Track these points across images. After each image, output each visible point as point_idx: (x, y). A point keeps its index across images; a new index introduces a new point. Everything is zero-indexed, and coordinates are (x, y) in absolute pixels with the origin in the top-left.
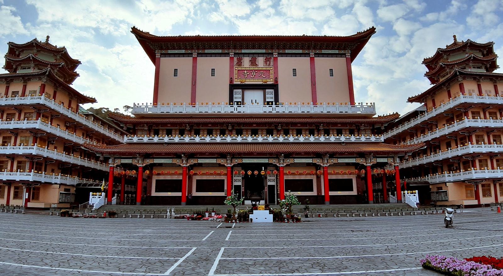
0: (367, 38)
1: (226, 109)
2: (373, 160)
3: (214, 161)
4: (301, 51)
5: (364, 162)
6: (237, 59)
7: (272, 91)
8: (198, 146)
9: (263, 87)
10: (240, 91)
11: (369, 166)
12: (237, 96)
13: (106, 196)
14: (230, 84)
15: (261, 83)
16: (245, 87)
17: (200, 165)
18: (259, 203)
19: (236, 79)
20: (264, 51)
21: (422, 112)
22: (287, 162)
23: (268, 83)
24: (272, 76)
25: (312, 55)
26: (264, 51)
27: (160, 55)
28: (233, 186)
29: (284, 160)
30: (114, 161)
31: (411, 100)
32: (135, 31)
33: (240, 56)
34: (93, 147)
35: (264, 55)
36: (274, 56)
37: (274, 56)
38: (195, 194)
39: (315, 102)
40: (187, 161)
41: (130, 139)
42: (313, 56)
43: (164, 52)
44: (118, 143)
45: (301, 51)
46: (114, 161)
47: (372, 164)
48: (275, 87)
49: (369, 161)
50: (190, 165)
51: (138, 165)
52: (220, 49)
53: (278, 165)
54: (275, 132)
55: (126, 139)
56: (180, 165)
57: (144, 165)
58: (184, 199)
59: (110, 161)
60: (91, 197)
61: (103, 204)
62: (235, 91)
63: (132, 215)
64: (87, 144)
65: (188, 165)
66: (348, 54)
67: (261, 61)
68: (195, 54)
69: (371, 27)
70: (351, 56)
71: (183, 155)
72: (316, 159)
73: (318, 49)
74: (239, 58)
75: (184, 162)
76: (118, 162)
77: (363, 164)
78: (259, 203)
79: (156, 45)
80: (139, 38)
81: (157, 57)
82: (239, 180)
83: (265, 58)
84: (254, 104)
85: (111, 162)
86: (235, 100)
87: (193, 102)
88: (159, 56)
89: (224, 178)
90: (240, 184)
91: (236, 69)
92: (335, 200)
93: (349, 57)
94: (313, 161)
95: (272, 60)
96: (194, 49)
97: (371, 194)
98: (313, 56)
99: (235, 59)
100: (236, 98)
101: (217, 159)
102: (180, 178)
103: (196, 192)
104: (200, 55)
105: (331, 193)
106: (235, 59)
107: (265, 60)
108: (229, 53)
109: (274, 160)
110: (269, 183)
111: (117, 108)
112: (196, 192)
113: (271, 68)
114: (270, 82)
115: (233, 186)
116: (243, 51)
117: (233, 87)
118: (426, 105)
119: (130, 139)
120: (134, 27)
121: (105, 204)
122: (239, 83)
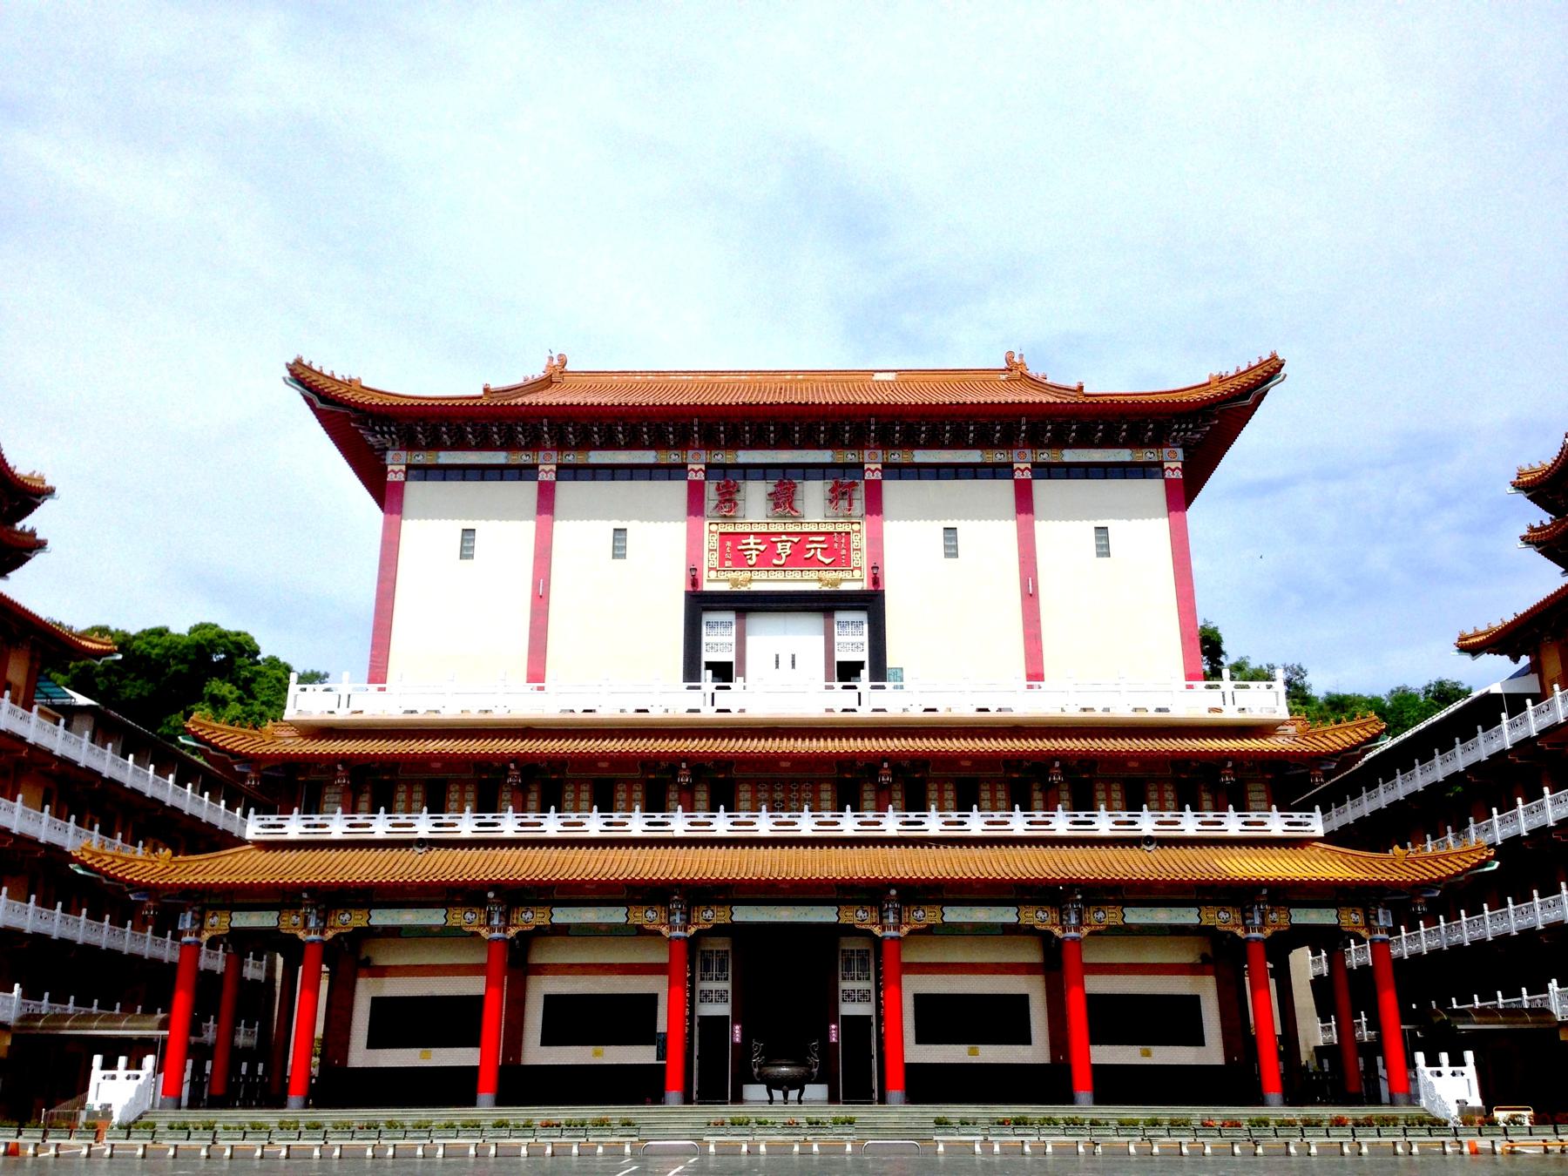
0: (1249, 401)
1: (672, 698)
2: (1274, 916)
3: (616, 916)
4: (499, 458)
5: (1236, 925)
6: (718, 489)
7: (862, 616)
8: (555, 853)
9: (825, 604)
10: (730, 617)
11: (1257, 939)
12: (718, 642)
13: (159, 1068)
14: (687, 593)
15: (815, 587)
16: (745, 605)
17: (563, 930)
18: (800, 1095)
19: (713, 574)
20: (824, 456)
21: (1515, 704)
22: (912, 920)
23: (844, 587)
24: (860, 559)
25: (547, 472)
26: (824, 456)
27: (406, 473)
28: (696, 1021)
29: (899, 913)
30: (200, 921)
31: (1471, 648)
32: (303, 377)
33: (730, 479)
34: (119, 862)
35: (828, 471)
36: (868, 476)
37: (868, 476)
38: (536, 1053)
39: (536, 675)
40: (506, 917)
41: (316, 826)
42: (878, 476)
43: (571, 458)
44: (228, 840)
45: (974, 456)
46: (202, 922)
47: (1269, 932)
48: (871, 603)
49: (1257, 921)
50: (519, 934)
51: (301, 935)
52: (649, 448)
53: (877, 930)
54: (868, 796)
55: (253, 828)
56: (476, 934)
57: (330, 934)
58: (488, 1078)
59: (186, 922)
60: (97, 1073)
61: (147, 1107)
62: (708, 617)
63: (288, 1147)
64: (94, 854)
65: (512, 932)
66: (1173, 465)
67: (813, 494)
68: (547, 468)
69: (1266, 357)
70: (1183, 471)
71: (491, 895)
72: (1033, 909)
73: (894, 447)
74: (727, 486)
75: (496, 922)
76: (218, 923)
77: (1233, 934)
78: (800, 1095)
79: (390, 433)
80: (319, 405)
81: (391, 477)
82: (721, 996)
83: (829, 484)
84: (785, 678)
85: (188, 926)
86: (707, 656)
87: (378, 674)
88: (401, 477)
89: (657, 985)
90: (723, 1009)
91: (714, 528)
92: (1117, 1087)
93: (1178, 475)
94: (1022, 915)
95: (860, 494)
96: (545, 449)
97: (1081, 1077)
98: (878, 476)
99: (711, 490)
100: (712, 647)
101: (632, 908)
102: (473, 986)
103: (543, 1044)
104: (570, 472)
105: (1104, 1055)
106: (711, 490)
107: (832, 491)
108: (535, 467)
109: (860, 913)
110: (847, 1009)
111: (1467, 657)
112: (543, 1044)
113: (856, 527)
114: (855, 582)
115: (696, 1021)
116: (745, 457)
117: (699, 604)
118: (1535, 667)
119: (316, 826)
120: (299, 362)
121: (153, 1106)
122: (725, 587)
